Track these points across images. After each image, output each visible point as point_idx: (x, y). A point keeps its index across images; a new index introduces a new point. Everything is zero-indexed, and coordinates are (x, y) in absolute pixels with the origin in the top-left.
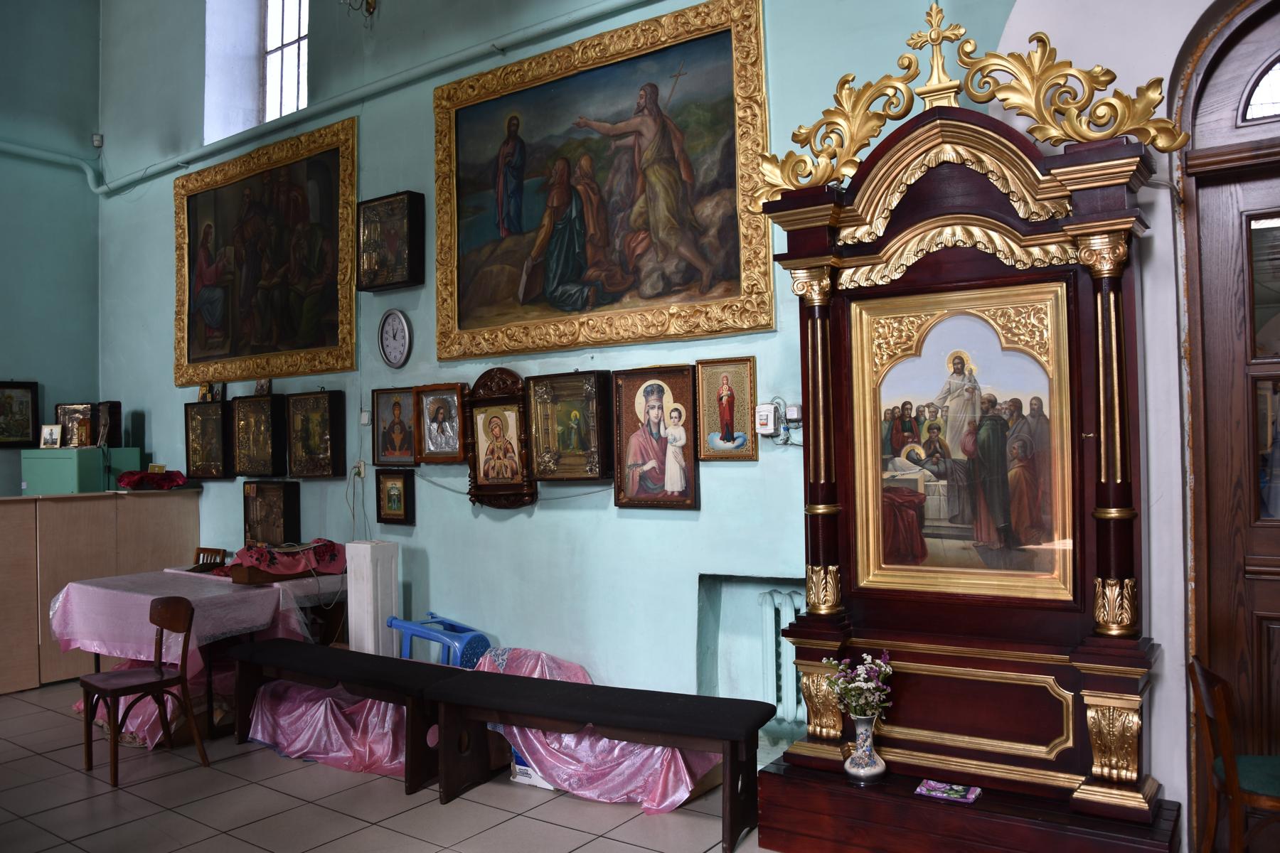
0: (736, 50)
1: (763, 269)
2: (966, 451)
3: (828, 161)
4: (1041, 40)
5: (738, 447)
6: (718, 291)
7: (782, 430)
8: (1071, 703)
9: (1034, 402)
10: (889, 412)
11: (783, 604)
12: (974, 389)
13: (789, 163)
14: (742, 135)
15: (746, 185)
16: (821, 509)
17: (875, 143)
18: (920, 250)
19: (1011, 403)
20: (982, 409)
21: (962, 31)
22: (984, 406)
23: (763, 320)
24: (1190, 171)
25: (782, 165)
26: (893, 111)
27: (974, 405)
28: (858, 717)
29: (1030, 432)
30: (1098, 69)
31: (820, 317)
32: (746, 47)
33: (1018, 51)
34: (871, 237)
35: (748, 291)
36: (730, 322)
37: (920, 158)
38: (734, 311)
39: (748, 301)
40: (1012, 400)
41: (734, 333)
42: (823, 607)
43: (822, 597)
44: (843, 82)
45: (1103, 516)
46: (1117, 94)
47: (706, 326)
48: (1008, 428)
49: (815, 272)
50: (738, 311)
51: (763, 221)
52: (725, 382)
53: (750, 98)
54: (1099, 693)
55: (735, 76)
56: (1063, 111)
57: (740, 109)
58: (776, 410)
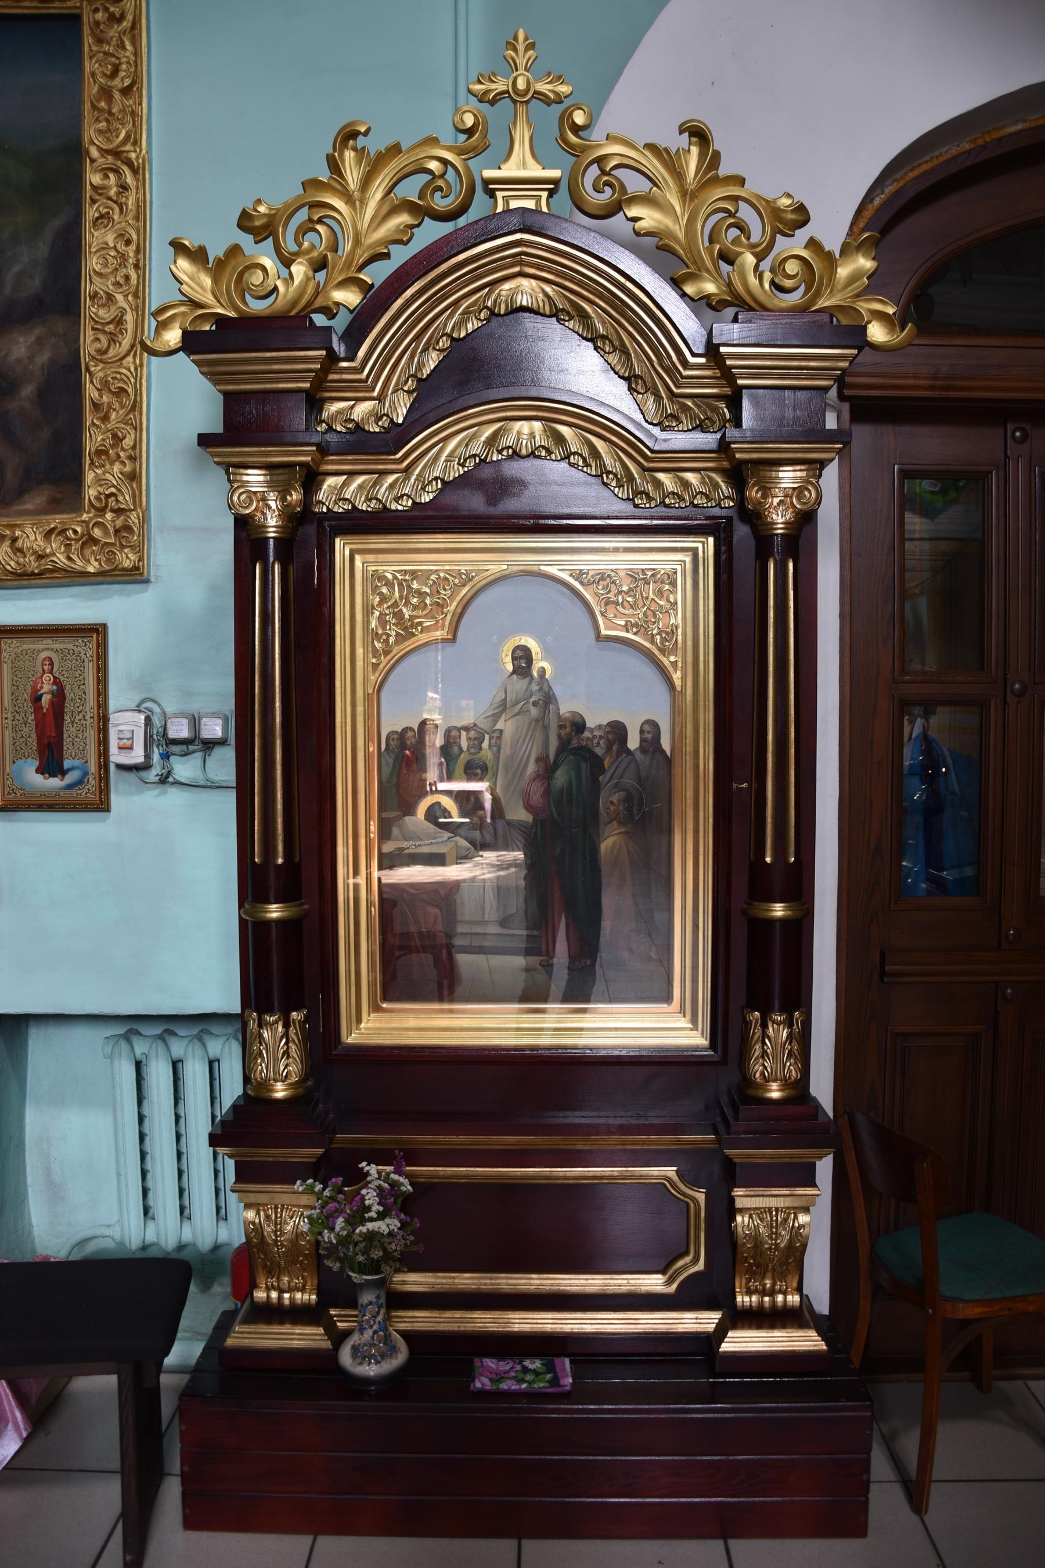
0: (91, 58)
1: (128, 468)
2: (531, 806)
3: (311, 273)
4: (699, 134)
5: (70, 787)
6: (37, 500)
7: (156, 757)
8: (703, 1206)
9: (647, 727)
10: (395, 736)
11: (153, 1054)
12: (548, 699)
13: (229, 269)
14: (98, 219)
15: (101, 312)
16: (275, 912)
17: (400, 255)
18: (470, 457)
19: (608, 729)
20: (559, 736)
21: (564, 89)
22: (563, 732)
23: (127, 559)
24: (847, 392)
25: (217, 270)
26: (440, 203)
27: (546, 728)
28: (365, 1277)
29: (639, 779)
30: (785, 202)
31: (277, 558)
32: (113, 55)
33: (662, 144)
34: (380, 423)
35: (98, 505)
36: (61, 559)
37: (478, 295)
38: (68, 539)
39: (97, 524)
40: (609, 724)
41: (68, 580)
42: (279, 1086)
43: (282, 1068)
44: (348, 135)
45: (762, 915)
46: (813, 244)
47: (12, 563)
48: (603, 771)
49: (282, 476)
50: (77, 540)
51: (132, 380)
52: (46, 668)
53: (116, 154)
54: (760, 1191)
55: (87, 106)
56: (732, 257)
57: (96, 171)
58: (148, 720)
